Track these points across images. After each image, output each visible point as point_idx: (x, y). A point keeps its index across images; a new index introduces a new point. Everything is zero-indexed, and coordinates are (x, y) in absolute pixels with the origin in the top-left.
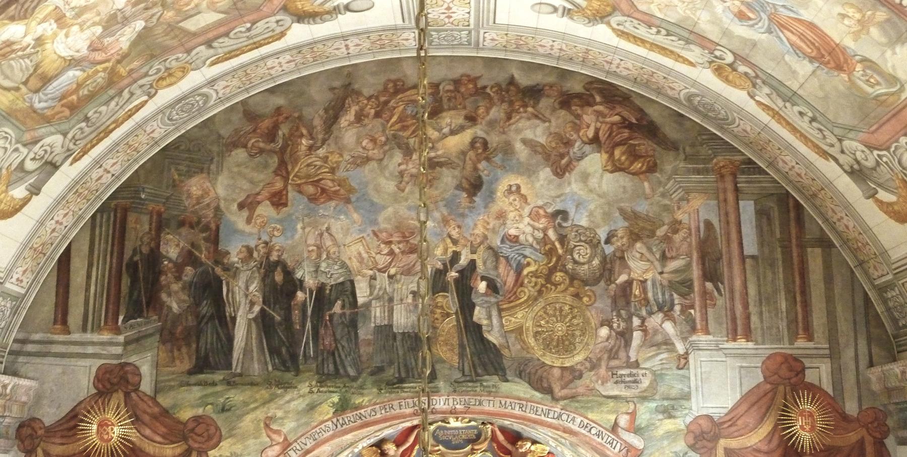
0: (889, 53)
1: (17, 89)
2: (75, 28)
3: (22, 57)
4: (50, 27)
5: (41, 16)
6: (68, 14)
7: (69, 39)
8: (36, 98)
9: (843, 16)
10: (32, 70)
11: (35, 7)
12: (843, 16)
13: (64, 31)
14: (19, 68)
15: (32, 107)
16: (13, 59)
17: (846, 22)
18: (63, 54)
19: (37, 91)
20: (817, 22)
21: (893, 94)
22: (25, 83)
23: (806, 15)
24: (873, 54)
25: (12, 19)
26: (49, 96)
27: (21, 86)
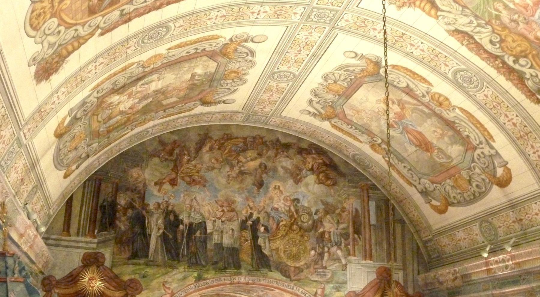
0: (450, 147)
9: (435, 131)
12: (435, 131)
17: (436, 134)
20: (423, 133)
21: (448, 162)
23: (419, 129)
24: (443, 146)
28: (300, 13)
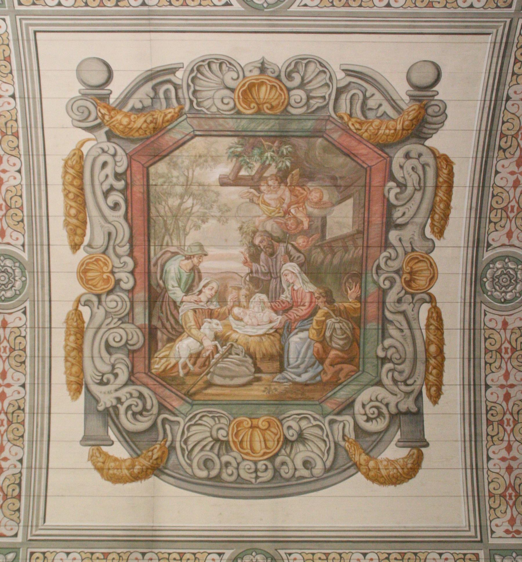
1: (258, 379)
2: (236, 310)
3: (224, 356)
4: (211, 327)
5: (192, 323)
6: (212, 307)
7: (246, 319)
8: (289, 374)
10: (250, 360)
11: (177, 321)
13: (231, 318)
14: (237, 367)
15: (296, 383)
16: (216, 363)
18: (261, 332)
19: (282, 369)
22: (258, 370)
25: (171, 340)
26: (303, 366)
27: (257, 375)
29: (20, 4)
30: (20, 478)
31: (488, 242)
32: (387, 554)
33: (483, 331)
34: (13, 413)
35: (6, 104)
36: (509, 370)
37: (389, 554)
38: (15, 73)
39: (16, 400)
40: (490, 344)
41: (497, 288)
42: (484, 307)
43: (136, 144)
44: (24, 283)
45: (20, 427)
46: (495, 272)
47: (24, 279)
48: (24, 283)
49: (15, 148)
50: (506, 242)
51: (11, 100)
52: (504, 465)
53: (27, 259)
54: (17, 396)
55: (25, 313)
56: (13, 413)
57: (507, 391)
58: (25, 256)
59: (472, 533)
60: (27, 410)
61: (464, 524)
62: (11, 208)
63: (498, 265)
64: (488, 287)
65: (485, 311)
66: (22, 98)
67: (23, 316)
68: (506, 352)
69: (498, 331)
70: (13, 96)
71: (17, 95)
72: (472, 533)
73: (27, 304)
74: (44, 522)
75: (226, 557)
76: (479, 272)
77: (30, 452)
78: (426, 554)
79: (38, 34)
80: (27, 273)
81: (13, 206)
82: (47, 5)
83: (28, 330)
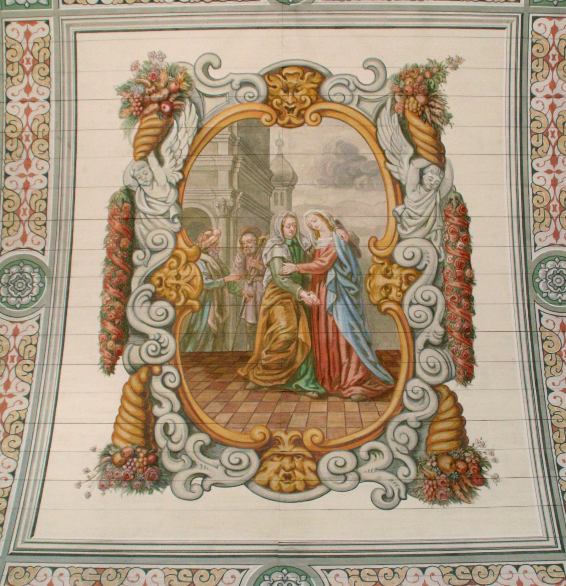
28: (550, 24)
29: (64, 3)
30: (9, 493)
31: (557, 464)
32: (453, 568)
33: (539, 333)
34: (12, 423)
35: (41, 108)
36: (550, 113)
37: (455, 569)
38: (53, 75)
39: (17, 411)
40: (538, 201)
41: (552, 289)
42: (538, 307)
43: (173, 125)
44: (41, 290)
45: (17, 438)
46: (547, 272)
47: (41, 285)
48: (41, 290)
49: (45, 152)
50: (554, 241)
51: (47, 104)
52: (548, 102)
53: (47, 264)
54: (18, 407)
55: (38, 321)
56: (12, 423)
57: (554, 167)
58: (46, 260)
59: (551, 542)
60: (28, 420)
61: (540, 533)
62: (35, 212)
63: (549, 264)
64: (542, 286)
65: (539, 311)
66: (58, 101)
67: (36, 325)
68: (555, 207)
69: (557, 333)
70: (48, 100)
71: (53, 98)
72: (551, 542)
73: (42, 311)
74: (32, 535)
75: (250, 574)
76: (530, 271)
77: (25, 463)
78: (500, 566)
79: (78, 35)
80: (46, 279)
81: (37, 210)
82: (88, 3)
83: (40, 338)
